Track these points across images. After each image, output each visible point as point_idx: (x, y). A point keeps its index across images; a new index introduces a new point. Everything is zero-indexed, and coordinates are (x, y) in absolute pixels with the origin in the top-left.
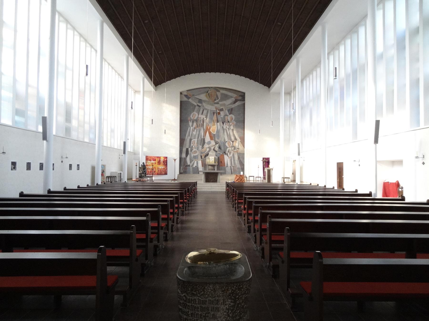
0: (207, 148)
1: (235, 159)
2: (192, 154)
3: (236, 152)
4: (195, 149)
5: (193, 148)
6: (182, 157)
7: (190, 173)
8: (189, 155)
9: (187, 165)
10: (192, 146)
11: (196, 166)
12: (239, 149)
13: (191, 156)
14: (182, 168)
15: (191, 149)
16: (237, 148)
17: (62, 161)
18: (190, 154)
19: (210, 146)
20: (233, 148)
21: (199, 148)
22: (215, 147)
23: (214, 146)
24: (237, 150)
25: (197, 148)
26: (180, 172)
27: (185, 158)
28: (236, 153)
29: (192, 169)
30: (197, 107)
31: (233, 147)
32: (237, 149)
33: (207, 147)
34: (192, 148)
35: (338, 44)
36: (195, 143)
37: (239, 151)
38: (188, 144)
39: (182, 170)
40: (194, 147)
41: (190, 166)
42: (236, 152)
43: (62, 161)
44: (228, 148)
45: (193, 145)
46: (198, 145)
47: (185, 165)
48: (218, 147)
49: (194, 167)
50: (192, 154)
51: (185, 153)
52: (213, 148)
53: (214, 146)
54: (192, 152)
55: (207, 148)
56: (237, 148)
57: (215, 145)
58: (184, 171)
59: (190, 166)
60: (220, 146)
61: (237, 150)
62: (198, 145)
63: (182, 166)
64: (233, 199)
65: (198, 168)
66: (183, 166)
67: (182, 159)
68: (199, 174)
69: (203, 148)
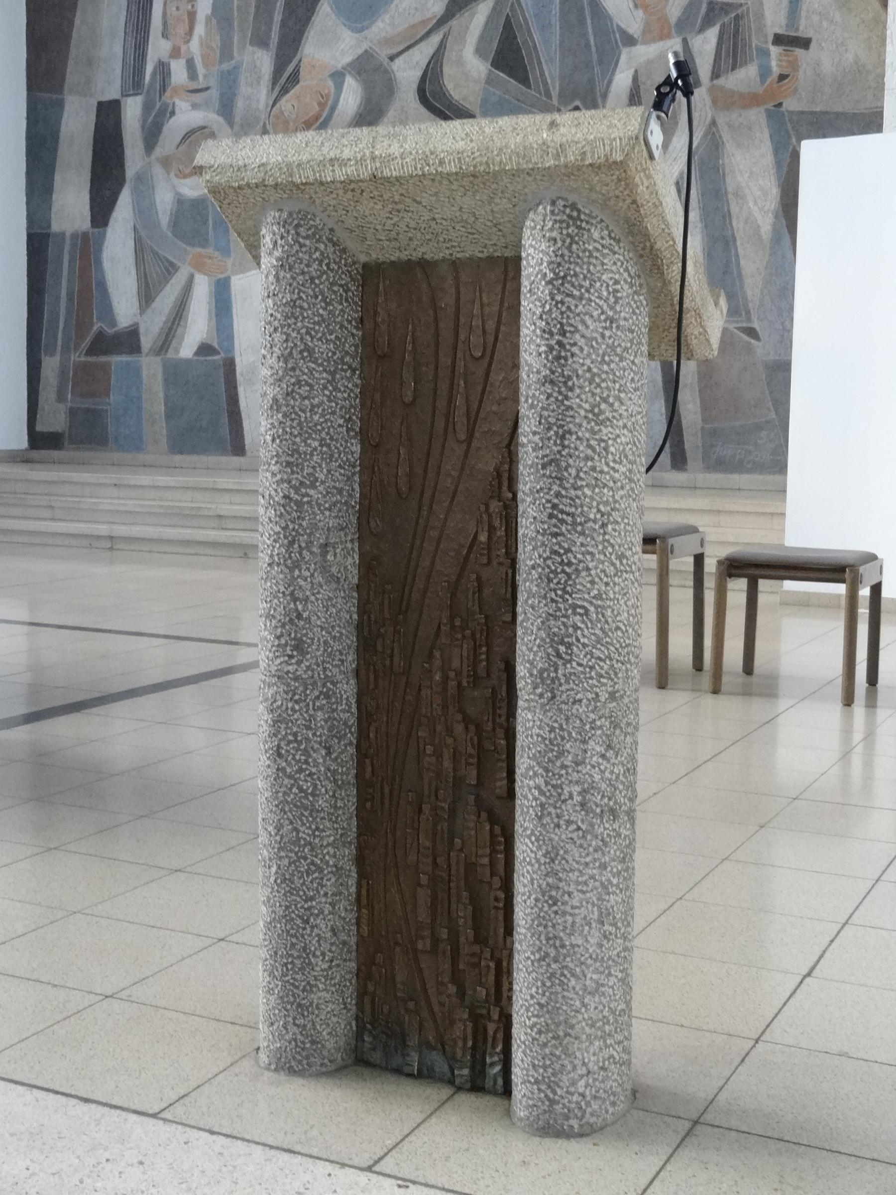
0: (338, 77)
1: (737, 224)
2: (158, 171)
3: (751, 100)
4: (195, 106)
5: (175, 91)
6: (55, 227)
7: (135, 444)
8: (125, 200)
9: (110, 331)
10: (163, 69)
11: (205, 349)
12: (805, 43)
13: (153, 204)
14: (50, 365)
15: (147, 107)
16: (779, 40)
17: (787, 76)
18: (140, 178)
19: (387, 42)
20: (712, 34)
21: (243, 78)
22: (442, 46)
23: (436, 39)
24: (775, 68)
25: (214, 94)
26: (39, 428)
27: (85, 236)
28: (757, 116)
29: (167, 381)
30: (607, 537)
31: (708, 22)
32: (774, 50)
33: (339, 65)
34: (164, 88)
35: (145, 466)
36: (192, 16)
37: (805, 73)
38: (118, 49)
39: (61, 398)
40: (178, 73)
41: (135, 348)
42: (751, 100)
43: (787, 76)
44: (625, 55)
45: (176, 53)
46: (226, 52)
47: (81, 325)
48: (480, 51)
49: (187, 361)
50: (158, 171)
51: (86, 176)
52: (416, 74)
53: (436, 39)
54: (158, 152)
55: (338, 77)
56: (779, 40)
57: (443, 20)
58: (72, 412)
59: (146, 342)
60: (508, 24)
61: (764, 72)
62: (226, 52)
63: (52, 355)
64: (568, 514)
65: (230, 366)
66: (66, 349)
67: (51, 252)
68: (236, 460)
69: (294, 79)
